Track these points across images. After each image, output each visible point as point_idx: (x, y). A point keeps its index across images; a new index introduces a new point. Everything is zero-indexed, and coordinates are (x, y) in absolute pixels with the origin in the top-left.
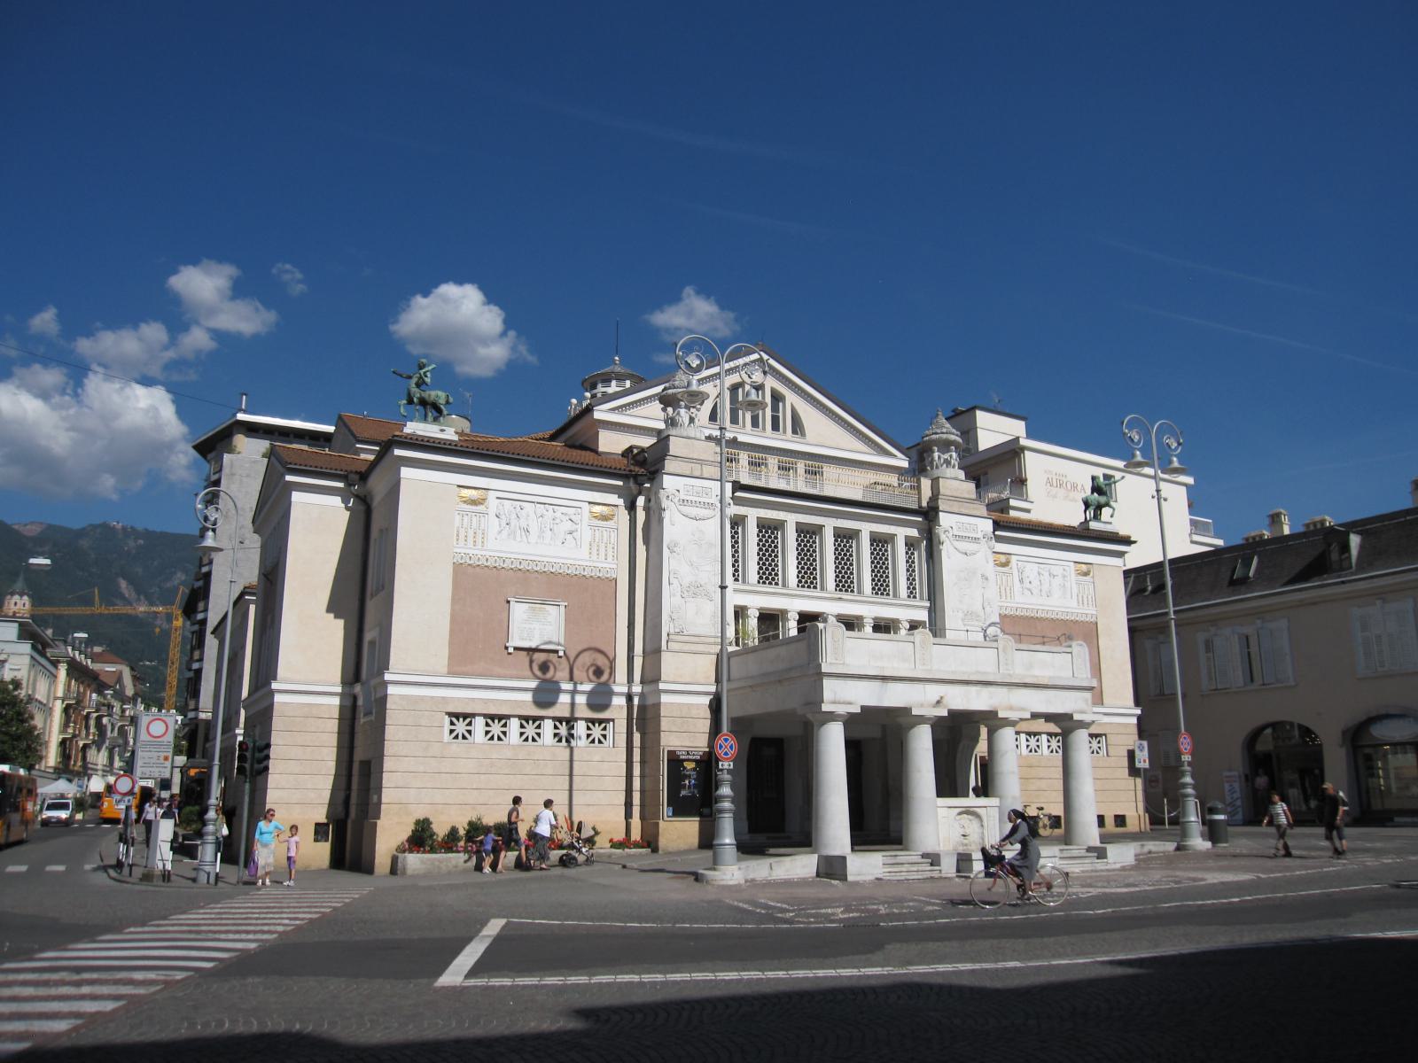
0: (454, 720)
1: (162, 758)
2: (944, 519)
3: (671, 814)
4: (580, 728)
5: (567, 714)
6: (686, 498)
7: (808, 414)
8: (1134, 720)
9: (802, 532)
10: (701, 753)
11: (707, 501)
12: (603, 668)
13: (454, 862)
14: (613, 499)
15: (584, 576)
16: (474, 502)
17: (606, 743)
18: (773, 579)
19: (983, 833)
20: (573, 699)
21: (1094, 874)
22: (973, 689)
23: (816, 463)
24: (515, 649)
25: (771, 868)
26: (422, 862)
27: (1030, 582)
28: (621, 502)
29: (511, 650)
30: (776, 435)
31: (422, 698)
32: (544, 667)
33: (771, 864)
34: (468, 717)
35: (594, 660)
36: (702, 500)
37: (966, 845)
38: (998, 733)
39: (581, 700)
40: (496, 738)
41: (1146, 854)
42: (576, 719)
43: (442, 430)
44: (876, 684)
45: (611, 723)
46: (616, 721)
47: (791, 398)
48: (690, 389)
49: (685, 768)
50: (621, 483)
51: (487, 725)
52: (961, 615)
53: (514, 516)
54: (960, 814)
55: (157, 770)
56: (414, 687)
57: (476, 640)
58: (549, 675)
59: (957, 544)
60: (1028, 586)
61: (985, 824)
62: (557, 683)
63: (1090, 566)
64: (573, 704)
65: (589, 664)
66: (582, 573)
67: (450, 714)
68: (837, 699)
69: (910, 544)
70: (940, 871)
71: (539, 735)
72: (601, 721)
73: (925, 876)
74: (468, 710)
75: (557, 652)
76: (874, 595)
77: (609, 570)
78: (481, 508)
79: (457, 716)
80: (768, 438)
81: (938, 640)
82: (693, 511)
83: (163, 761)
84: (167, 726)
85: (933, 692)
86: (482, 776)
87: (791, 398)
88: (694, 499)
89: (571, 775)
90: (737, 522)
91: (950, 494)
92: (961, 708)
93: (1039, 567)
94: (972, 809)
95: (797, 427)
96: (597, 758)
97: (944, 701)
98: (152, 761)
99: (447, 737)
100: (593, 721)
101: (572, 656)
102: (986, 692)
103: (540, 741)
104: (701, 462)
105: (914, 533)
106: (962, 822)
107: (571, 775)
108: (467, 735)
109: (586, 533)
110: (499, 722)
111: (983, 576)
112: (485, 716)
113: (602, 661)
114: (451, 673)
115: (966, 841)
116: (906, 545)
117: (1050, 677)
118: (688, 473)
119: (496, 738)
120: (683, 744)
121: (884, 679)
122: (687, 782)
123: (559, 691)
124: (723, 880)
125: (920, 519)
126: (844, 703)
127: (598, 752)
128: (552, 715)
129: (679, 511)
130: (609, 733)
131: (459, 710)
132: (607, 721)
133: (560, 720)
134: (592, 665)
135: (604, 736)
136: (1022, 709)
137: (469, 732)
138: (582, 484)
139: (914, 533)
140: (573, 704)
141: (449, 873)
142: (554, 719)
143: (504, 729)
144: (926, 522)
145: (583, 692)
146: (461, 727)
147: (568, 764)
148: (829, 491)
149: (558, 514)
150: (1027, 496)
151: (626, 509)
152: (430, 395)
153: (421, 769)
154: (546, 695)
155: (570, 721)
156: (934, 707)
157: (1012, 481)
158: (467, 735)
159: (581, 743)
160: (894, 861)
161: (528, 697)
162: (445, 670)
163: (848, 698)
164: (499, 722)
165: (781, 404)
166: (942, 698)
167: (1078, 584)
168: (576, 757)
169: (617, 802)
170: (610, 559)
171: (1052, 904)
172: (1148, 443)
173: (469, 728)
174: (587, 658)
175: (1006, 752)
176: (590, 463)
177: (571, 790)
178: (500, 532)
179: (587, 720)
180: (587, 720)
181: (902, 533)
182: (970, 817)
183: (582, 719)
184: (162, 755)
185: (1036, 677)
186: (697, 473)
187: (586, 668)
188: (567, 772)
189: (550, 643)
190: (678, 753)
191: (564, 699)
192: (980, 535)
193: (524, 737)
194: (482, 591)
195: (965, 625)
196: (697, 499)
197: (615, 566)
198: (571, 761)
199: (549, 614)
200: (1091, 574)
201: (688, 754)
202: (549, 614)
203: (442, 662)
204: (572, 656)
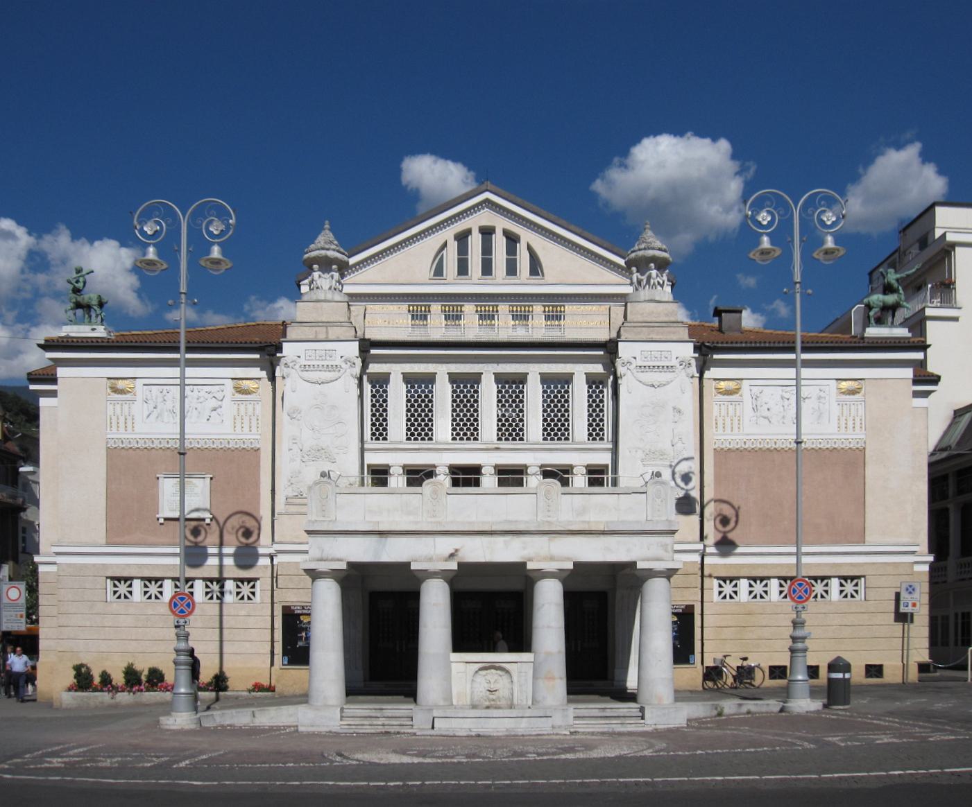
0: (116, 582)
1: (19, 616)
2: (624, 349)
3: (286, 663)
4: (230, 585)
5: (216, 575)
6: (307, 363)
7: (549, 252)
8: (926, 568)
9: (594, 382)
10: (683, 607)
11: (330, 363)
12: (252, 529)
13: (100, 699)
14: (256, 372)
15: (229, 449)
16: (122, 392)
17: (857, 597)
18: (563, 435)
19: (512, 689)
20: (221, 561)
21: (554, 737)
22: (500, 540)
23: (555, 303)
24: (166, 519)
25: (254, 716)
26: (74, 698)
27: (768, 409)
28: (263, 374)
29: (162, 521)
30: (512, 280)
31: (85, 566)
32: (196, 532)
33: (253, 712)
34: (159, 580)
35: (243, 522)
36: (325, 363)
37: (493, 700)
38: (647, 582)
39: (229, 562)
40: (153, 597)
41: (744, 714)
42: (225, 579)
43: (93, 329)
44: (373, 540)
45: (863, 579)
46: (867, 577)
47: (527, 236)
48: (147, 258)
49: (301, 622)
50: (257, 356)
51: (751, 586)
52: (640, 454)
53: (160, 399)
54: (481, 669)
55: (17, 624)
56: (134, 556)
57: (128, 514)
58: (200, 538)
59: (306, 375)
60: (766, 413)
61: (515, 679)
62: (205, 548)
63: (863, 382)
64: (221, 566)
65: (238, 527)
66: (227, 446)
67: (112, 578)
68: (325, 556)
69: (594, 382)
70: (412, 725)
71: (826, 592)
72: (249, 580)
73: (378, 731)
74: (125, 574)
75: (204, 520)
76: (591, 441)
77: (253, 441)
78: (128, 396)
79: (119, 579)
80: (500, 284)
81: (566, 489)
82: (315, 375)
83: (19, 618)
84: (7, 595)
85: (445, 545)
86: (140, 630)
87: (527, 236)
88: (316, 363)
89: (221, 628)
90: (381, 381)
91: (640, 320)
92: (482, 560)
93: (782, 391)
94: (497, 665)
95: (536, 267)
96: (243, 613)
97: (460, 554)
98: (13, 618)
99: (110, 596)
100: (242, 580)
101: (221, 521)
102: (517, 542)
103: (737, 598)
104: (327, 324)
105: (598, 368)
106: (488, 677)
107: (221, 628)
108: (764, 595)
109: (229, 409)
110: (851, 582)
111: (674, 408)
112: (142, 579)
113: (250, 523)
114: (108, 544)
115: (491, 697)
116: (588, 382)
117: (607, 522)
118: (311, 337)
119: (153, 597)
120: (300, 600)
121: (382, 534)
122: (304, 634)
123: (236, 556)
124: (167, 725)
125: (602, 353)
126: (332, 560)
127: (246, 607)
128: (172, 576)
129: (301, 377)
130: (861, 588)
131: (118, 575)
132: (255, 579)
133: (211, 580)
134: (241, 527)
135: (253, 594)
136: (568, 559)
137: (766, 592)
138: (128, 362)
139: (598, 368)
140: (221, 566)
141: (96, 708)
142: (204, 579)
143: (856, 588)
144: (702, 357)
145: (228, 555)
146: (123, 588)
147: (218, 618)
148: (571, 335)
149: (203, 393)
150: (955, 302)
151: (269, 380)
152: (83, 299)
153: (88, 624)
154: (195, 556)
155: (221, 581)
156: (446, 561)
157: (932, 287)
158: (764, 595)
159: (228, 598)
160: (600, 714)
161: (177, 561)
162: (104, 541)
163: (338, 555)
164: (851, 582)
165: (518, 245)
166: (457, 550)
167: (839, 403)
168: (225, 612)
169: (262, 651)
170: (254, 430)
171: (129, 758)
172: (786, 225)
173: (129, 589)
174: (235, 522)
175: (543, 605)
176: (230, 341)
177: (221, 641)
178: (148, 416)
179: (235, 579)
180: (235, 579)
181: (580, 372)
182: (499, 672)
183: (230, 579)
184: (19, 613)
185: (588, 522)
186: (322, 337)
187: (235, 530)
188: (217, 625)
189: (197, 510)
190: (292, 608)
191: (213, 561)
192: (674, 362)
193: (753, 595)
194: (131, 470)
195: (644, 465)
196: (320, 363)
197: (258, 437)
198: (221, 616)
199: (197, 487)
200: (863, 392)
201: (303, 609)
202: (197, 487)
203: (101, 536)
204: (221, 521)
